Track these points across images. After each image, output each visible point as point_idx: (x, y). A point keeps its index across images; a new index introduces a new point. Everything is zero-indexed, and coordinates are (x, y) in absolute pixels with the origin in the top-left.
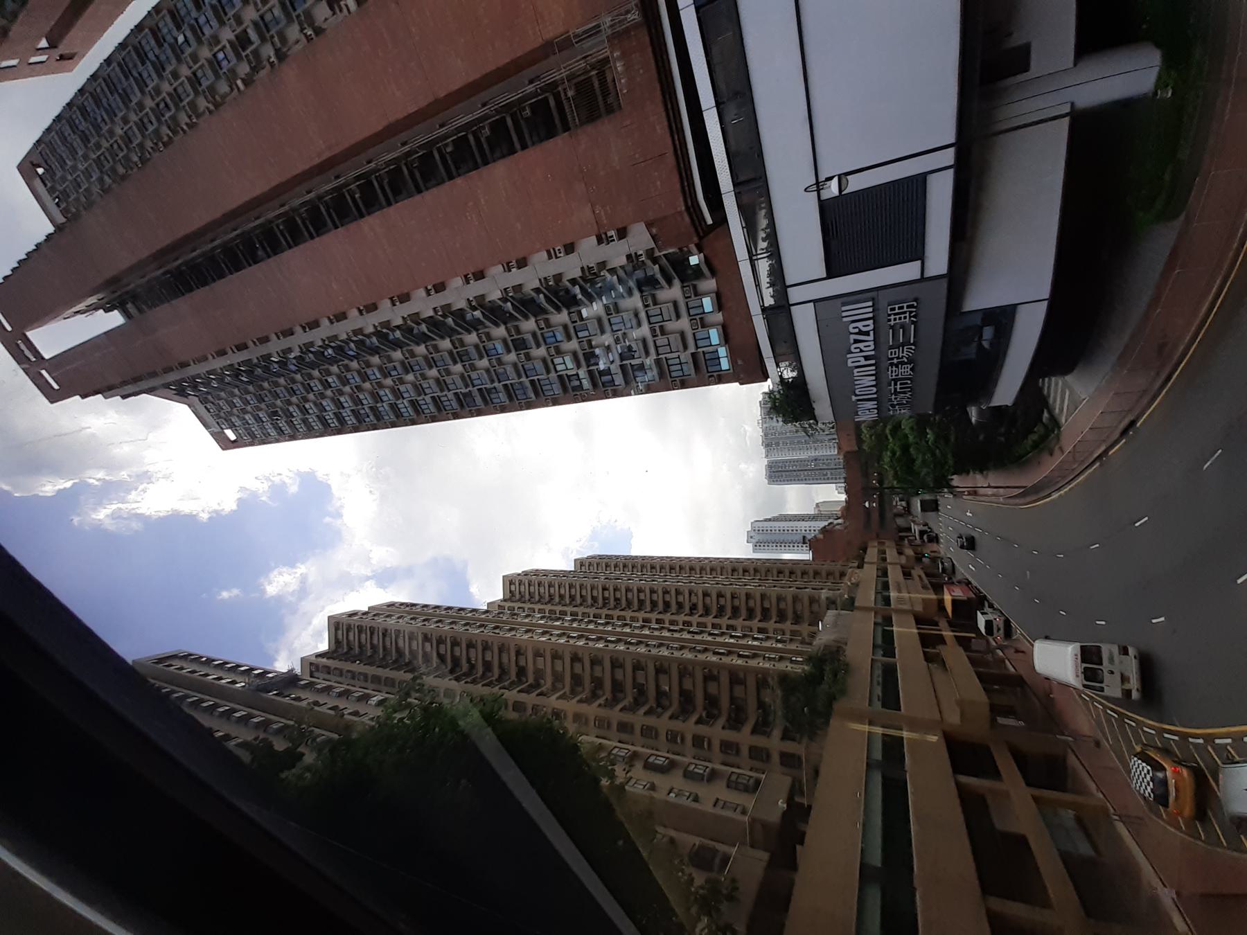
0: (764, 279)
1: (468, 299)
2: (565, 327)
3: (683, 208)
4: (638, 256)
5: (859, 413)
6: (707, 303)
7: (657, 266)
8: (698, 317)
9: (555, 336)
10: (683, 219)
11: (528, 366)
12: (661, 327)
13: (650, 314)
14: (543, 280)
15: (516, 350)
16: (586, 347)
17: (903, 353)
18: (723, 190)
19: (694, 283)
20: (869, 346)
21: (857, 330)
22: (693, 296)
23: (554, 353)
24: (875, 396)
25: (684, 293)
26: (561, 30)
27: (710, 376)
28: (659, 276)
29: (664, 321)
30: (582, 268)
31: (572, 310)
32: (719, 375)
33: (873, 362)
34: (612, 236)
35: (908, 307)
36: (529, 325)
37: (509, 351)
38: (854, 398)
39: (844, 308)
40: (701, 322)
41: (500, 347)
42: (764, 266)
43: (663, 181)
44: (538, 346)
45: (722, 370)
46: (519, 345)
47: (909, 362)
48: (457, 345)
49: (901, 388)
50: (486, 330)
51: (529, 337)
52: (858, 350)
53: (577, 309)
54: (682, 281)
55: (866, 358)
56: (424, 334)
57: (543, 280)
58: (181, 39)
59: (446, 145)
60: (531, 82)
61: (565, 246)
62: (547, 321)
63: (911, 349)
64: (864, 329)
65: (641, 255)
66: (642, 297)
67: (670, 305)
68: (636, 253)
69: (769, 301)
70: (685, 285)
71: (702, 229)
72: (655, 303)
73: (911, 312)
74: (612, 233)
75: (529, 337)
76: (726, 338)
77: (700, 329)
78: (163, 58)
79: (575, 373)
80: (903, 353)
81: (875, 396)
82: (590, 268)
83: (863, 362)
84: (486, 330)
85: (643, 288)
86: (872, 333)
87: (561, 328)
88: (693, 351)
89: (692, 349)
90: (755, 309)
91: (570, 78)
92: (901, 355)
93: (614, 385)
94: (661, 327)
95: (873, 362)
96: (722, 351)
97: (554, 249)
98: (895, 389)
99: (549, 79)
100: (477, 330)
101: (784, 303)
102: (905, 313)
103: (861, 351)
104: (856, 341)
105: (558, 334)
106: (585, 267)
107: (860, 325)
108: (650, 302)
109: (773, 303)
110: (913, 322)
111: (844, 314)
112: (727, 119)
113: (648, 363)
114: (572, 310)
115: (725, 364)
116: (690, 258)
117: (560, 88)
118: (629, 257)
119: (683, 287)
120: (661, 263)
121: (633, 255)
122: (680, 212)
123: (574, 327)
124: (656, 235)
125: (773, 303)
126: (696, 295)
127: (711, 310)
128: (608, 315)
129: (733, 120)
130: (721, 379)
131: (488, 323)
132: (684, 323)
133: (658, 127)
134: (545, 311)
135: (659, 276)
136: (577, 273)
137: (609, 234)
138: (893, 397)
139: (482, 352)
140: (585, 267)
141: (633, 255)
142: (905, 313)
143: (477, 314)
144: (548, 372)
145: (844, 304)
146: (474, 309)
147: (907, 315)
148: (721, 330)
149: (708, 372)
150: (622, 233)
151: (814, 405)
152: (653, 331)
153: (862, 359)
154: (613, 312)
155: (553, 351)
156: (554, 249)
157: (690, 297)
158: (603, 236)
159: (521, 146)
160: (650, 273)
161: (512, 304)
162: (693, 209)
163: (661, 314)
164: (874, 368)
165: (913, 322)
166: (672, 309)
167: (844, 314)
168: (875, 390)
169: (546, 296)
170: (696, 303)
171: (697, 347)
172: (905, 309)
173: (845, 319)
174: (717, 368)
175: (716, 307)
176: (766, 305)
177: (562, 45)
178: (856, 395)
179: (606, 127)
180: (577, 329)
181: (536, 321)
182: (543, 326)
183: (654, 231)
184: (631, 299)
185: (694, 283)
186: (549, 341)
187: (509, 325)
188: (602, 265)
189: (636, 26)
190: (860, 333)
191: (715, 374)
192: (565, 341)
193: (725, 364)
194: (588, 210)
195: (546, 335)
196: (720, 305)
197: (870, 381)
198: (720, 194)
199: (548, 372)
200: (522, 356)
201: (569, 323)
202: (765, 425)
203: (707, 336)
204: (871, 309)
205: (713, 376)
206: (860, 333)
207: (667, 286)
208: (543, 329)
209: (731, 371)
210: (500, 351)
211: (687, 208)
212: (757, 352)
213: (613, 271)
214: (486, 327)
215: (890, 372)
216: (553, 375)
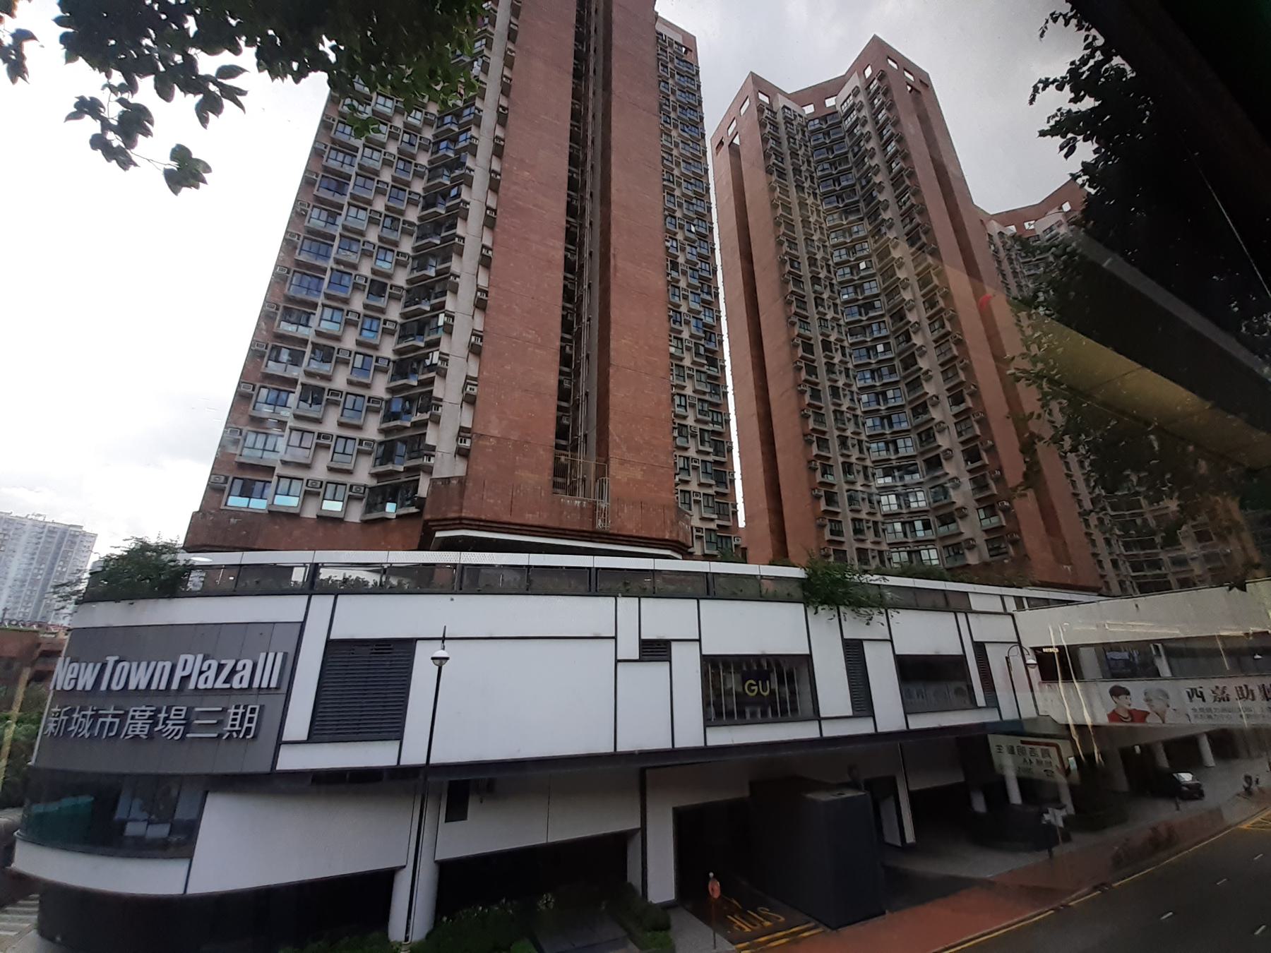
0: (354, 574)
1: (459, 277)
2: (375, 347)
3: (463, 515)
4: (429, 457)
5: (76, 665)
6: (333, 507)
7: (402, 470)
8: (322, 491)
9: (370, 330)
10: (455, 512)
11: (346, 280)
12: (328, 447)
13: (349, 441)
14: (447, 357)
15: (372, 281)
16: (340, 355)
17: (174, 725)
18: (464, 554)
19: (364, 500)
20: (209, 680)
21: (239, 667)
22: (351, 493)
23: (349, 317)
24: (103, 687)
25: (359, 486)
26: (611, 473)
27: (227, 478)
28: (390, 467)
29: (334, 452)
30: (441, 400)
31: (391, 364)
32: (223, 490)
33: (175, 686)
34: (465, 442)
35: (249, 729)
36: (394, 312)
37: (374, 272)
38: (111, 660)
39: (280, 656)
40: (313, 492)
41: (386, 266)
42: (371, 578)
43: (492, 506)
44: (366, 306)
45: (229, 495)
46: (378, 287)
47: (150, 735)
48: (406, 226)
49: (175, 715)
50: (409, 267)
51: (381, 303)
52: (205, 668)
53: (390, 372)
54: (371, 489)
55: (185, 679)
56: (434, 205)
57: (447, 357)
58: (693, 229)
59: (571, 348)
60: (585, 436)
61: (475, 397)
62: (392, 333)
63: (176, 735)
64: (237, 678)
65: (429, 460)
66: (374, 441)
67: (350, 467)
68: (434, 456)
69: (324, 574)
70: (367, 490)
71: (433, 526)
72: (360, 452)
73: (238, 732)
74: (468, 444)
75: (381, 303)
76: (275, 515)
77: (305, 488)
78: (691, 208)
79: (311, 324)
80: (174, 725)
81: (103, 687)
82: (437, 407)
83: (179, 674)
84: (409, 267)
85: (383, 447)
86: (227, 686)
87: (377, 342)
88: (276, 472)
89: (279, 470)
90: (321, 556)
91: (573, 462)
92: (171, 722)
93: (269, 360)
94: (328, 447)
95: (175, 686)
96: (258, 504)
97: (476, 385)
98: (106, 716)
99: (581, 447)
100: (414, 258)
101: (317, 589)
102: (241, 725)
103: (201, 673)
104: (221, 667)
105: (371, 335)
106: (441, 403)
107: (247, 673)
108: (364, 447)
109: (322, 577)
110: (220, 736)
111: (271, 656)
112: (505, 572)
113: (283, 413)
114: (391, 364)
115: (236, 502)
116: (395, 505)
117: (569, 453)
118: (433, 448)
119: (365, 487)
120: (403, 475)
121: (433, 453)
122: (461, 511)
123: (372, 356)
124: (449, 482)
125: (322, 577)
126: (350, 498)
127: (324, 508)
128: (369, 398)
129: (509, 576)
130: (215, 489)
131: (416, 274)
132: (320, 472)
133: (531, 515)
134: (402, 338)
135: (390, 467)
136: (437, 392)
137: (468, 441)
138: (89, 713)
139: (388, 245)
140: (441, 403)
141: (433, 453)
142: (241, 725)
143: (432, 272)
144: (328, 296)
145: (285, 655)
146: (438, 273)
147: (237, 728)
148: (292, 511)
149: (234, 478)
150: (462, 453)
151: (123, 604)
152: (327, 436)
153: (186, 673)
154: (371, 404)
155: (352, 317)
156: (476, 385)
157: (307, 485)
158: (469, 435)
159: (561, 407)
160: (397, 459)
161: (426, 312)
162: (460, 523)
163: (344, 453)
164: (163, 687)
165: (220, 736)
166: (346, 467)
167: (271, 656)
168: (264, 685)
169: (419, 348)
170: (340, 494)
171: (280, 477)
172: (246, 725)
173: (263, 655)
174: (328, 495)
175: (324, 514)
176: (322, 570)
177: (602, 471)
178: (117, 662)
179: (547, 476)
180: (367, 358)
181: (396, 322)
182: (387, 326)
183: (454, 482)
184: (376, 430)
185: (364, 500)
186: (368, 321)
187: (404, 293)
188: (436, 420)
189: (594, 523)
190: (233, 672)
191: (228, 486)
192: (359, 338)
193: (236, 502)
194: (495, 432)
195: (375, 323)
196: (326, 520)
197: (139, 679)
198: (594, 555)
199: (328, 296)
200: (363, 282)
201: (379, 354)
202: (30, 523)
203: (291, 493)
204: (114, 687)
205: (226, 482)
206: (233, 672)
207: (374, 471)
208: (385, 324)
209: (222, 507)
210: (379, 263)
211: (460, 519)
212: (264, 548)
213: (424, 424)
214: (413, 269)
215: (143, 708)
216: (321, 300)
